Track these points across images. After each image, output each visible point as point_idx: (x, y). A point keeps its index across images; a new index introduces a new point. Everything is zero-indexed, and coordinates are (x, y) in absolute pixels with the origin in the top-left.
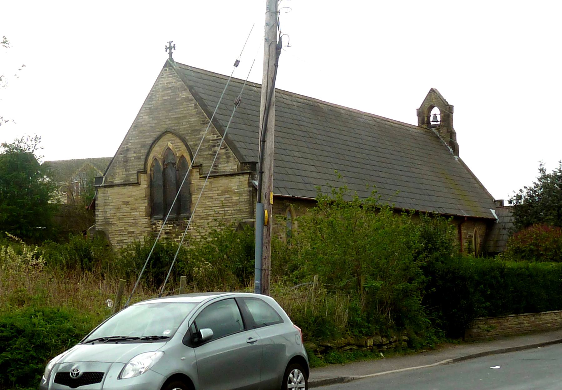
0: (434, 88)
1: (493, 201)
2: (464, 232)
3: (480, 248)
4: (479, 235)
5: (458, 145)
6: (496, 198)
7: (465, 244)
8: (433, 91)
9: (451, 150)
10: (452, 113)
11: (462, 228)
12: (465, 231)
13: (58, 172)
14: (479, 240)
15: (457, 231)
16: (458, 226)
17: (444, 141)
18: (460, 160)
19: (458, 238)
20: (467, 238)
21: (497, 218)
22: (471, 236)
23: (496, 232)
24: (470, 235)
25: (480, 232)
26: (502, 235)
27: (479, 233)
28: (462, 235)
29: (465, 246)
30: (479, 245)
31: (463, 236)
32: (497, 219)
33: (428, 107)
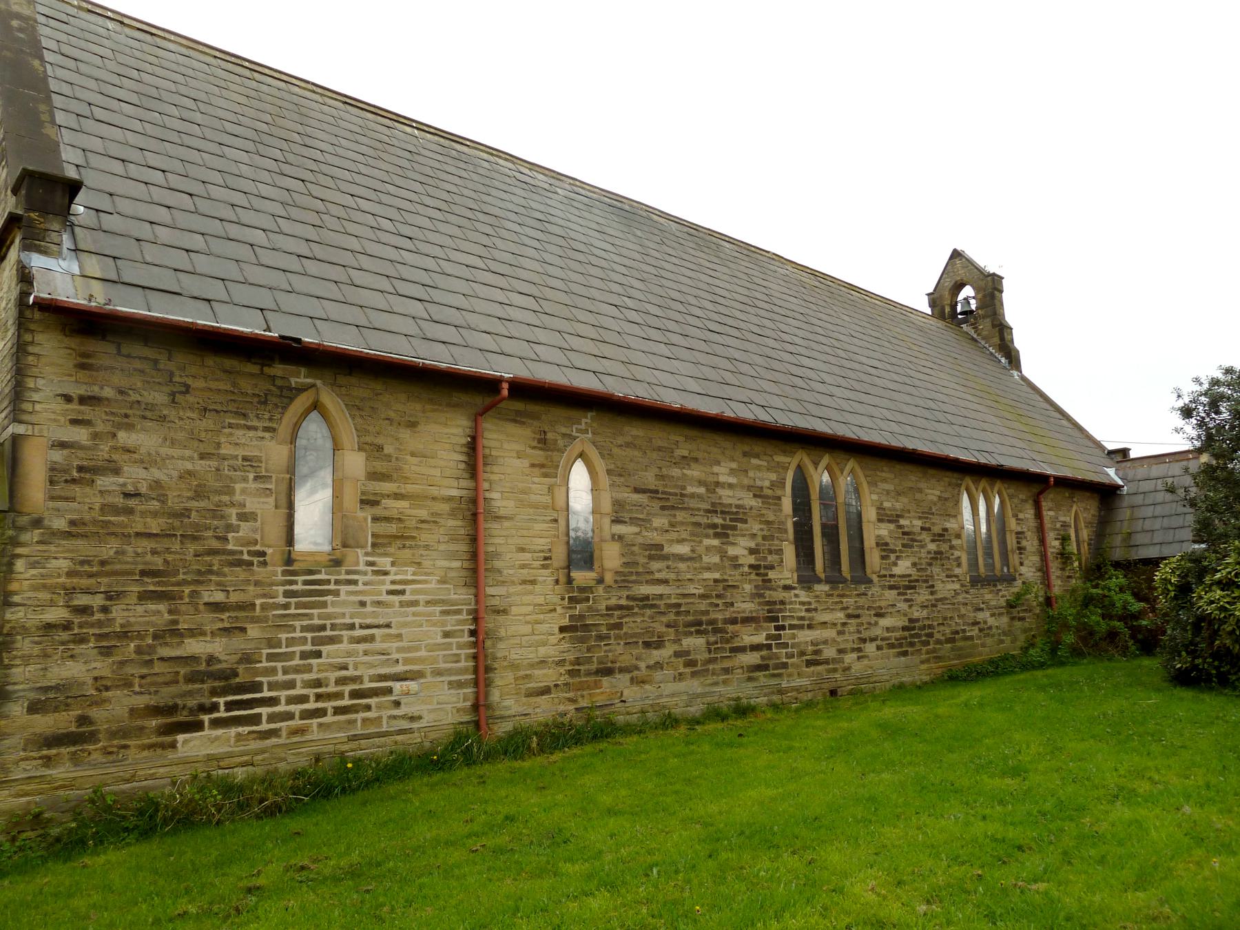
0: (959, 249)
1: (1106, 452)
2: (1048, 514)
3: (1090, 553)
4: (1085, 523)
5: (1018, 352)
6: (1111, 447)
7: (1054, 544)
8: (956, 254)
9: (1003, 360)
10: (1001, 292)
11: (1045, 505)
12: (1051, 513)
13: (877, 486)
14: (1085, 534)
15: (1032, 512)
16: (1035, 501)
17: (987, 345)
18: (1024, 379)
19: (1035, 530)
20: (1058, 530)
21: (1120, 482)
22: (1065, 525)
23: (1124, 514)
24: (1065, 522)
25: (1085, 515)
26: (1141, 521)
27: (1085, 518)
28: (1045, 521)
29: (1054, 547)
30: (1086, 544)
31: (1048, 525)
32: (1123, 487)
33: (950, 286)
